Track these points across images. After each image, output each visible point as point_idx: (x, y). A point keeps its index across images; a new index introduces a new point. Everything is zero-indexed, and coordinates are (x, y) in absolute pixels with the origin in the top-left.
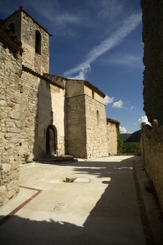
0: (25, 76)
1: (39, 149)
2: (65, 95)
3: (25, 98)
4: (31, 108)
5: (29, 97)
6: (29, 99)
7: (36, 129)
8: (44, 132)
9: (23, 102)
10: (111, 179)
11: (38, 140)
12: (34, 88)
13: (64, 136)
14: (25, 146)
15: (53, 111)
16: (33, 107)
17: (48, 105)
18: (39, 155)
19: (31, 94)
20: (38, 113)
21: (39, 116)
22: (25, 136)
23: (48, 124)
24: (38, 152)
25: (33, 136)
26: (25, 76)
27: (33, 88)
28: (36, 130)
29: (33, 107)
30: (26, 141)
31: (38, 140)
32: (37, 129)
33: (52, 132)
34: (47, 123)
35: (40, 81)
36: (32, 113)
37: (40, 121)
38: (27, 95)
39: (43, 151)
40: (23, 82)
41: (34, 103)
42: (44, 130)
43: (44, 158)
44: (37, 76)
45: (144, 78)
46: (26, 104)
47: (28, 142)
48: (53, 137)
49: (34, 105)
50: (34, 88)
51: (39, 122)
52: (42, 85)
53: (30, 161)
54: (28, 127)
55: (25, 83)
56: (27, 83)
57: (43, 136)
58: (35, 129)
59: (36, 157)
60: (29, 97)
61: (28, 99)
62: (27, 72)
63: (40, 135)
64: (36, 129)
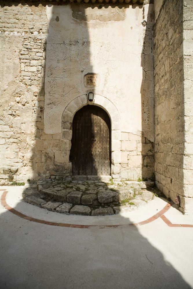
0: (11, 16)
1: (46, 160)
2: (146, 19)
3: (11, 61)
4: (25, 77)
5: (22, 55)
6: (20, 59)
7: (41, 117)
8: (64, 122)
9: (6, 69)
10: (71, 163)
11: (45, 140)
12: (36, 33)
13: (141, 130)
14: (7, 152)
15: (95, 71)
16: (30, 74)
17: (78, 59)
18: (48, 172)
19: (27, 49)
20: (44, 84)
21: (47, 90)
22: (8, 133)
23: (77, 103)
24: (45, 167)
25: (29, 132)
26: (11, 16)
27: (32, 33)
28: (39, 119)
29: (30, 74)
30: (11, 143)
31: (45, 140)
32: (42, 117)
33: (103, 122)
34: (72, 103)
35: (53, 13)
36: (29, 87)
37: (50, 99)
38: (17, 53)
39: (59, 164)
40: (5, 29)
41: (34, 64)
42: (63, 117)
43: (59, 180)
44: (43, 5)
45: (7, 6)
46: (12, 71)
47: (15, 144)
48: (105, 134)
49: (34, 69)
50: (36, 33)
51: (47, 101)
52: (57, 19)
53: (21, 182)
54: (19, 116)
55: (11, 29)
56: (15, 29)
57: (60, 132)
58: (37, 119)
59: (37, 175)
60: (22, 55)
61: (17, 61)
62: (16, 5)
63: (48, 130)
64: (41, 117)
